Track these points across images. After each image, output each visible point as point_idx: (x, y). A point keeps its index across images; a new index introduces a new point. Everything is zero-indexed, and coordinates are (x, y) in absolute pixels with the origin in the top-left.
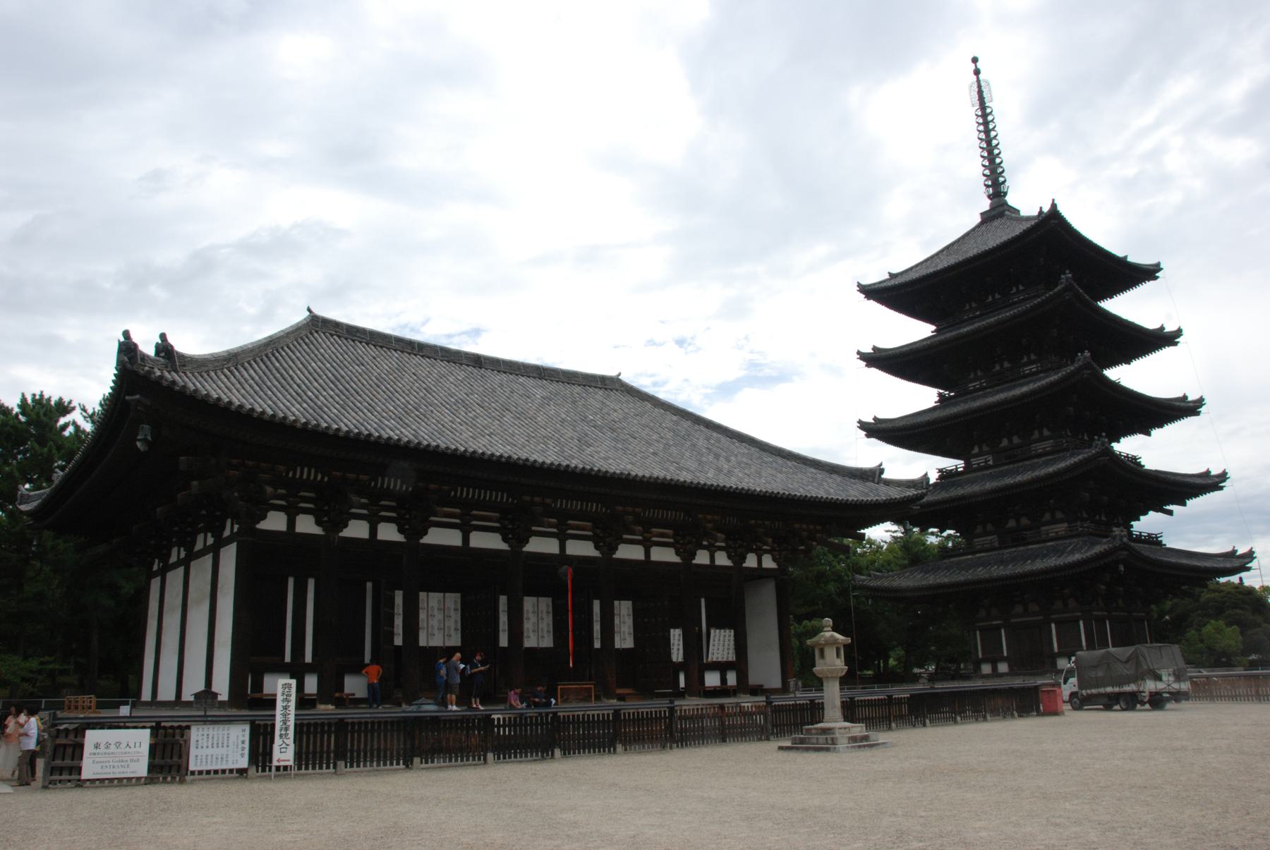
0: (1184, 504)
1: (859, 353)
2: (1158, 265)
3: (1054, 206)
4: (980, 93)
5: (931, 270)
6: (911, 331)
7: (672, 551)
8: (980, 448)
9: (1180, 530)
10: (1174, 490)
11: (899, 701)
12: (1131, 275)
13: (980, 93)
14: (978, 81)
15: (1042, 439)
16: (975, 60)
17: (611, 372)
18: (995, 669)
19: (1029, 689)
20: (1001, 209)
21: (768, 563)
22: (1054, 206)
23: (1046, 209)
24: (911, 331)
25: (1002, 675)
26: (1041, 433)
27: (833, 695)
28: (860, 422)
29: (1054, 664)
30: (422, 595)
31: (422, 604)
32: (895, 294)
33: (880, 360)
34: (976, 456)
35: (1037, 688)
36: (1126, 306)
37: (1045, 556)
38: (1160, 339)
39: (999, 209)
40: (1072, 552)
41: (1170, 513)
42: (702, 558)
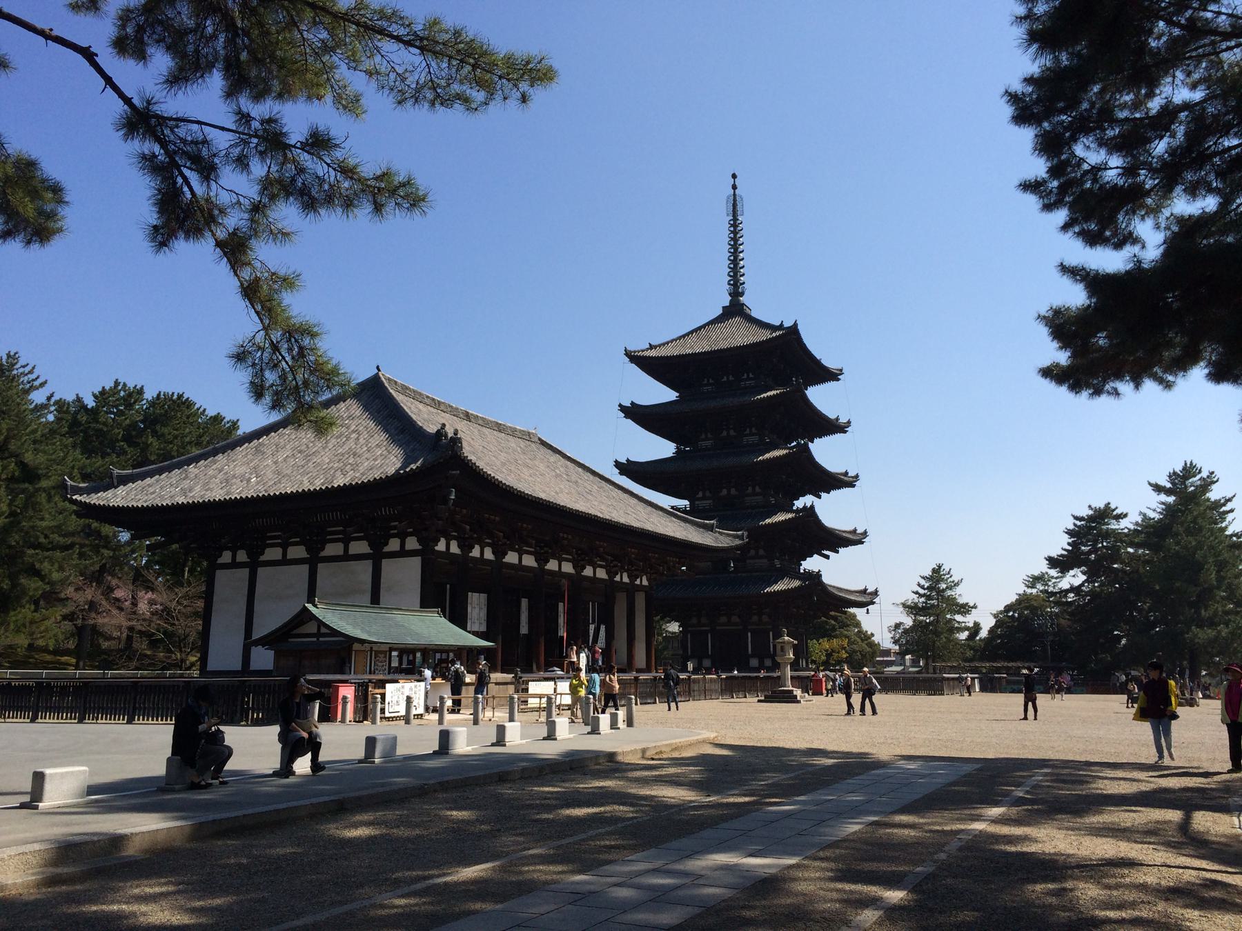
0: (837, 552)
1: (620, 405)
3: (795, 324)
9: (835, 570)
12: (827, 375)
13: (735, 205)
14: (734, 195)
15: (707, 439)
16: (734, 176)
21: (645, 582)
22: (795, 324)
33: (634, 413)
34: (699, 499)
38: (833, 427)
39: (735, 310)
41: (827, 557)
42: (476, 553)
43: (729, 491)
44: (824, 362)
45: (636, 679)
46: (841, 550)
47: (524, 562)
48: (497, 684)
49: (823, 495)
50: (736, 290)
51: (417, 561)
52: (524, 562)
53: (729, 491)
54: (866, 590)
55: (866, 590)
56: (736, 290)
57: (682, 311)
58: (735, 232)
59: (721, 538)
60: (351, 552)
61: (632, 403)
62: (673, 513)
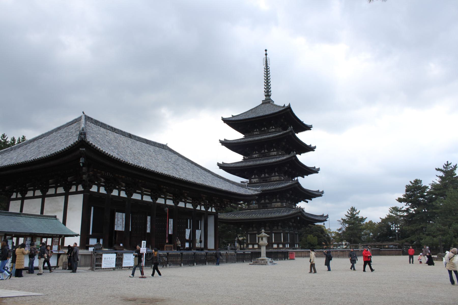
0: (311, 200)
1: (220, 140)
2: (312, 126)
3: (289, 105)
4: (266, 61)
5: (247, 117)
6: (236, 136)
7: (191, 205)
8: (255, 176)
9: (308, 207)
10: (309, 195)
11: (248, 254)
13: (266, 61)
14: (266, 57)
16: (266, 50)
17: (165, 143)
18: (253, 247)
19: (285, 252)
20: (268, 101)
21: (214, 210)
22: (289, 105)
23: (287, 105)
24: (236, 136)
25: (281, 248)
26: (275, 174)
27: (263, 250)
28: (218, 163)
29: (272, 246)
30: (117, 213)
31: (116, 216)
32: (232, 123)
33: (227, 144)
34: (253, 179)
35: (288, 252)
36: (302, 136)
37: (274, 213)
38: (309, 149)
39: (268, 101)
40: (283, 212)
41: (307, 202)
42: (198, 208)
43: (265, 175)
44: (305, 123)
45: (182, 253)
46: (313, 199)
47: (187, 207)
48: (82, 255)
49: (305, 177)
50: (268, 93)
51: (81, 196)
52: (187, 207)
53: (265, 175)
54: (323, 215)
55: (323, 215)
56: (268, 93)
57: (247, 102)
58: (267, 72)
59: (249, 191)
60: (58, 192)
61: (225, 139)
62: (241, 185)
